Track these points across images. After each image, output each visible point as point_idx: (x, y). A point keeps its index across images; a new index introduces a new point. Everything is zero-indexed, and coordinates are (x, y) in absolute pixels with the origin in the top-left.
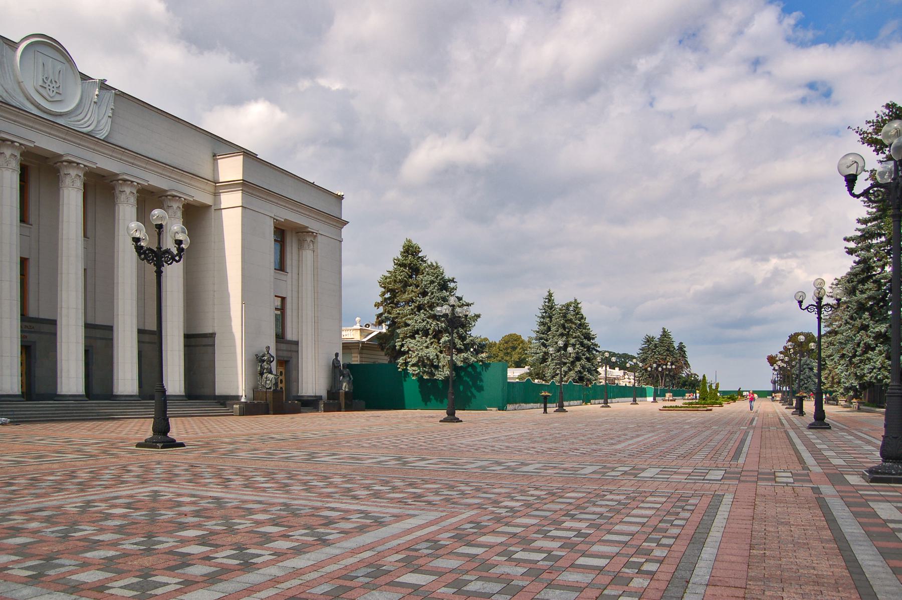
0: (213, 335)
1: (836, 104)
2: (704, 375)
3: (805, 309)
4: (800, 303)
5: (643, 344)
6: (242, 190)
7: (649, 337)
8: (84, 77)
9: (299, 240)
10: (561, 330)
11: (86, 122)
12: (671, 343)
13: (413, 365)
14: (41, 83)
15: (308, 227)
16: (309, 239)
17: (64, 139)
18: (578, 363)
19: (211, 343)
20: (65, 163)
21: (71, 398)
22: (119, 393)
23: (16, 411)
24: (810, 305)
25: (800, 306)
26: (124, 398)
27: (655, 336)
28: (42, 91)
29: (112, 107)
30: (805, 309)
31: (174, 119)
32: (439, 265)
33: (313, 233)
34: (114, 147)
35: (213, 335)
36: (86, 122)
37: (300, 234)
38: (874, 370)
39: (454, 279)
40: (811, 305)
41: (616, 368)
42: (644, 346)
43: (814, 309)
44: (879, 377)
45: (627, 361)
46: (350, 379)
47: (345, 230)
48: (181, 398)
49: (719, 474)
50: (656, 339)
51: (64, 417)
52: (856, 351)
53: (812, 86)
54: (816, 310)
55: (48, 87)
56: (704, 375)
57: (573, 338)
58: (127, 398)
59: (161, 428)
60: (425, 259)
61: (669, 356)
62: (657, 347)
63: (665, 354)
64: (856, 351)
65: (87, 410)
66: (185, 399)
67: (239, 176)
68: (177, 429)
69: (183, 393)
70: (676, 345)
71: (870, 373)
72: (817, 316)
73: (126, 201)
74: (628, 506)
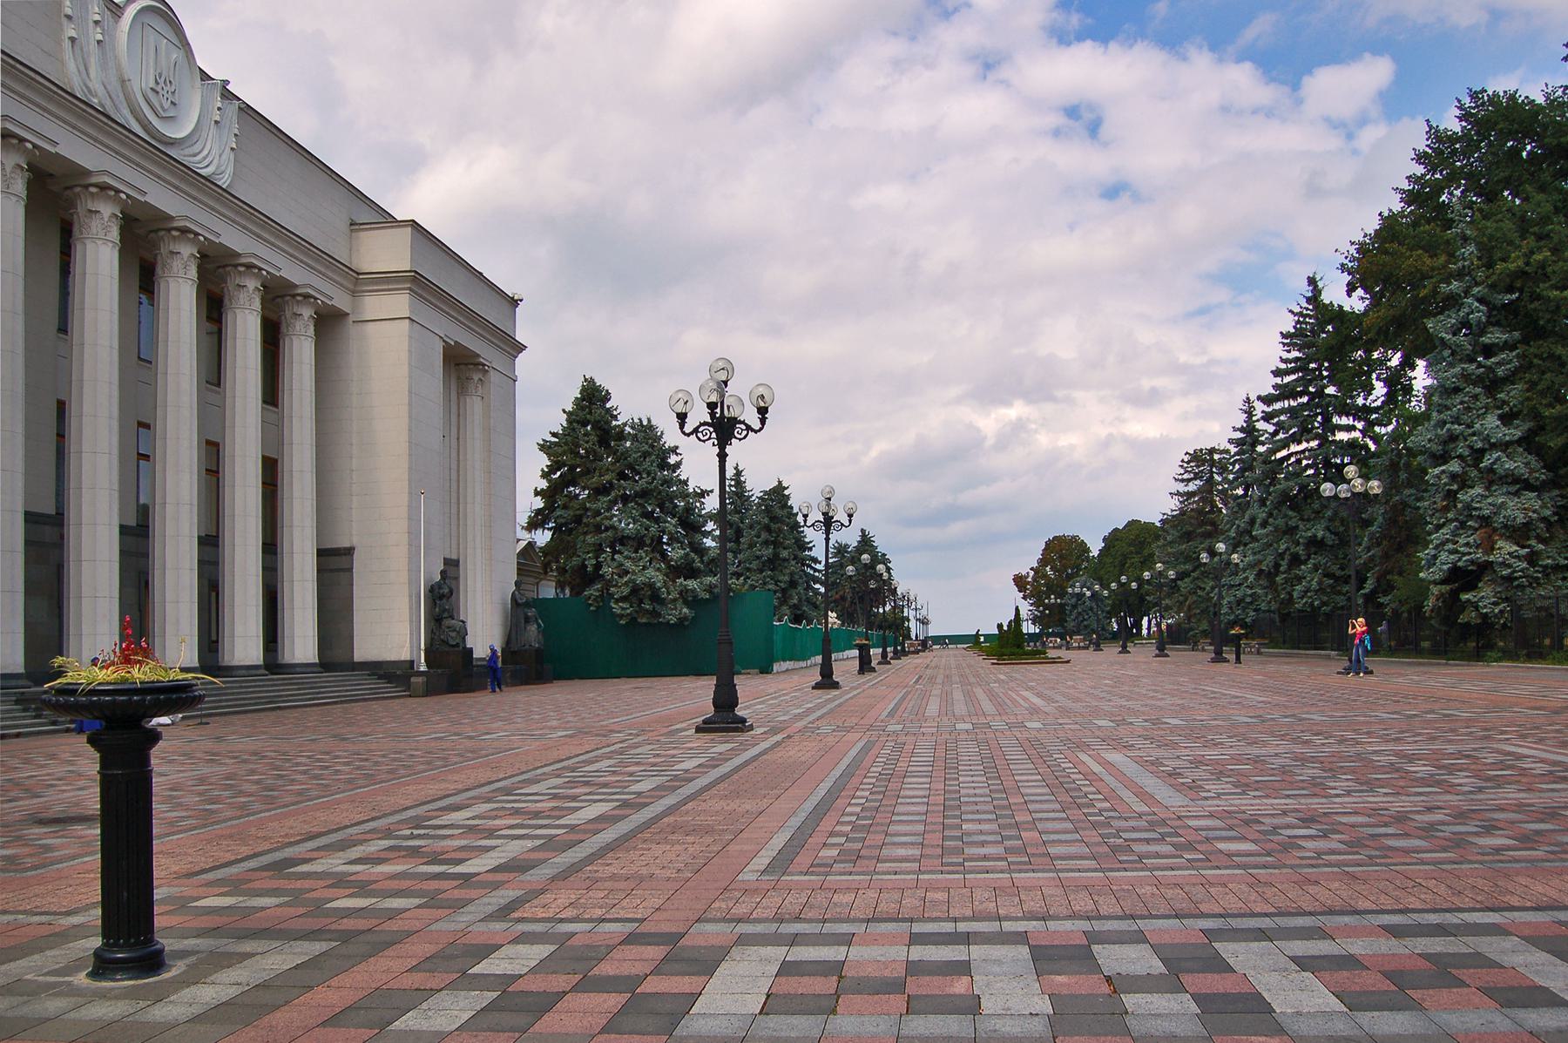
0: (349, 551)
1: (1106, 145)
3: (691, 433)
4: (682, 417)
6: (410, 289)
8: (205, 76)
9: (459, 378)
10: (764, 535)
11: (205, 158)
13: (623, 599)
14: (152, 84)
15: (478, 356)
16: (476, 378)
17: (177, 188)
18: (793, 592)
19: (347, 566)
20: (175, 233)
21: (309, 670)
22: (236, 663)
23: (237, 688)
25: (682, 426)
26: (244, 672)
28: (151, 95)
29: (236, 132)
30: (691, 433)
31: (290, 143)
32: (653, 423)
33: (484, 365)
34: (252, 211)
35: (349, 551)
36: (205, 158)
37: (461, 367)
38: (1309, 594)
39: (677, 447)
44: (1316, 603)
46: (539, 626)
47: (521, 360)
48: (315, 669)
51: (314, 699)
52: (1280, 565)
53: (1072, 112)
55: (161, 92)
57: (785, 548)
58: (254, 672)
60: (615, 413)
64: (1280, 565)
65: (233, 694)
66: (320, 669)
67: (406, 265)
69: (261, 662)
71: (1302, 598)
72: (716, 450)
73: (247, 303)
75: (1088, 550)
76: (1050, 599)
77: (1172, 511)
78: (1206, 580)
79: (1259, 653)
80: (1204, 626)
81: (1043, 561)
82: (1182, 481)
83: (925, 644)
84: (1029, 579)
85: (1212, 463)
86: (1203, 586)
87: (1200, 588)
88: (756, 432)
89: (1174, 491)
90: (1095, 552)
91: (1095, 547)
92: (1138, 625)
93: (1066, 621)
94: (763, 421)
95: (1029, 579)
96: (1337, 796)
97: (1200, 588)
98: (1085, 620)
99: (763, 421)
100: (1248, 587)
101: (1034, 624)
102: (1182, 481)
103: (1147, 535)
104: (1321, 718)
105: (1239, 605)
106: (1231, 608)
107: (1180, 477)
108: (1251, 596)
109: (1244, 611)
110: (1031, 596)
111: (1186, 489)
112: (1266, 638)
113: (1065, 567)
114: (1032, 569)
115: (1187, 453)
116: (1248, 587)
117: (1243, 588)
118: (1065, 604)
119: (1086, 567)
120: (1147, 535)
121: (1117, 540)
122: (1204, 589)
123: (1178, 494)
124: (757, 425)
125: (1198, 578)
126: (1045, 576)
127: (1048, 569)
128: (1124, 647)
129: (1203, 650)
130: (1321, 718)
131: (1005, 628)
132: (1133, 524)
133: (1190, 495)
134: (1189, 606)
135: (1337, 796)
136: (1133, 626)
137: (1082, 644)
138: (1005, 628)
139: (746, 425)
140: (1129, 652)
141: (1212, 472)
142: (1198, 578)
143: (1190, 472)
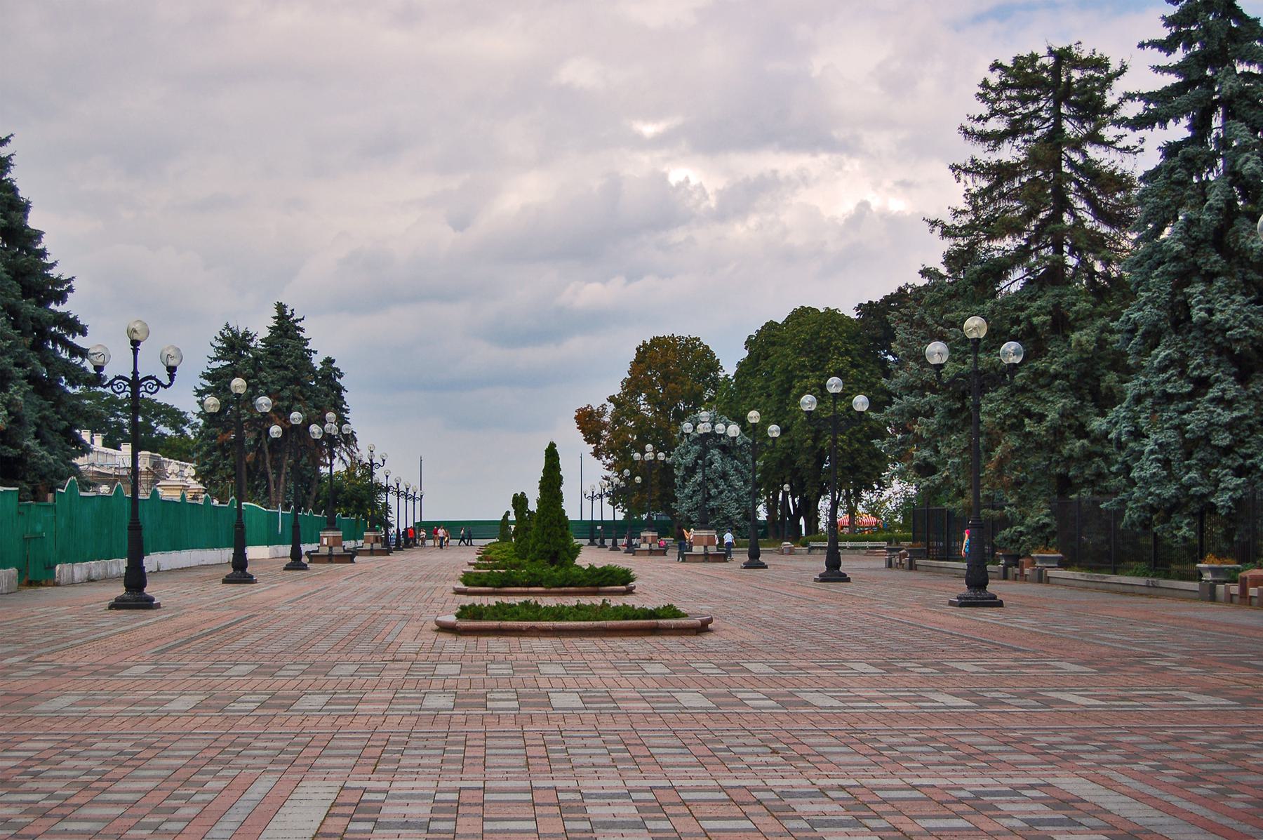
2: (552, 446)
5: (215, 359)
7: (235, 335)
12: (305, 356)
24: (117, 378)
27: (252, 330)
40: (120, 378)
41: (123, 446)
42: (217, 365)
43: (125, 386)
45: (153, 424)
49: (305, 704)
50: (257, 343)
54: (128, 388)
56: (552, 446)
59: (833, 563)
61: (299, 400)
62: (261, 369)
63: (286, 393)
68: (848, 564)
70: (317, 362)
74: (195, 770)
75: (714, 366)
76: (643, 452)
77: (957, 213)
78: (1044, 393)
79: (912, 567)
80: (1040, 514)
81: (634, 385)
82: (983, 137)
83: (408, 540)
84: (607, 419)
85: (1062, 93)
86: (1036, 409)
87: (1029, 414)
88: (166, 387)
89: (963, 160)
90: (729, 369)
91: (730, 358)
92: (808, 509)
93: (675, 500)
94: (172, 377)
95: (607, 419)
96: (1032, 787)
97: (1029, 414)
98: (710, 497)
99: (172, 377)
100: (1218, 401)
101: (613, 503)
102: (983, 137)
103: (834, 334)
104: (1084, 701)
105: (1189, 455)
106: (1166, 463)
107: (978, 127)
108: (1229, 427)
109: (1205, 475)
110: (611, 449)
111: (993, 158)
112: (338, 530)
113: (673, 397)
114: (611, 399)
115: (996, 66)
116: (1218, 401)
117: (1203, 403)
118: (673, 465)
119: (711, 399)
120: (834, 334)
121: (773, 344)
122: (1041, 418)
123: (975, 169)
124: (166, 381)
125: (1023, 389)
126: (635, 413)
127: (641, 399)
128: (977, 581)
129: (1041, 578)
130: (1084, 701)
131: (533, 506)
132: (802, 315)
133: (1002, 172)
134: (1001, 462)
135: (1032, 787)
136: (799, 512)
137: (655, 547)
138: (533, 506)
139: (157, 380)
140: (764, 566)
141: (1059, 117)
142: (1023, 389)
143: (1003, 113)
